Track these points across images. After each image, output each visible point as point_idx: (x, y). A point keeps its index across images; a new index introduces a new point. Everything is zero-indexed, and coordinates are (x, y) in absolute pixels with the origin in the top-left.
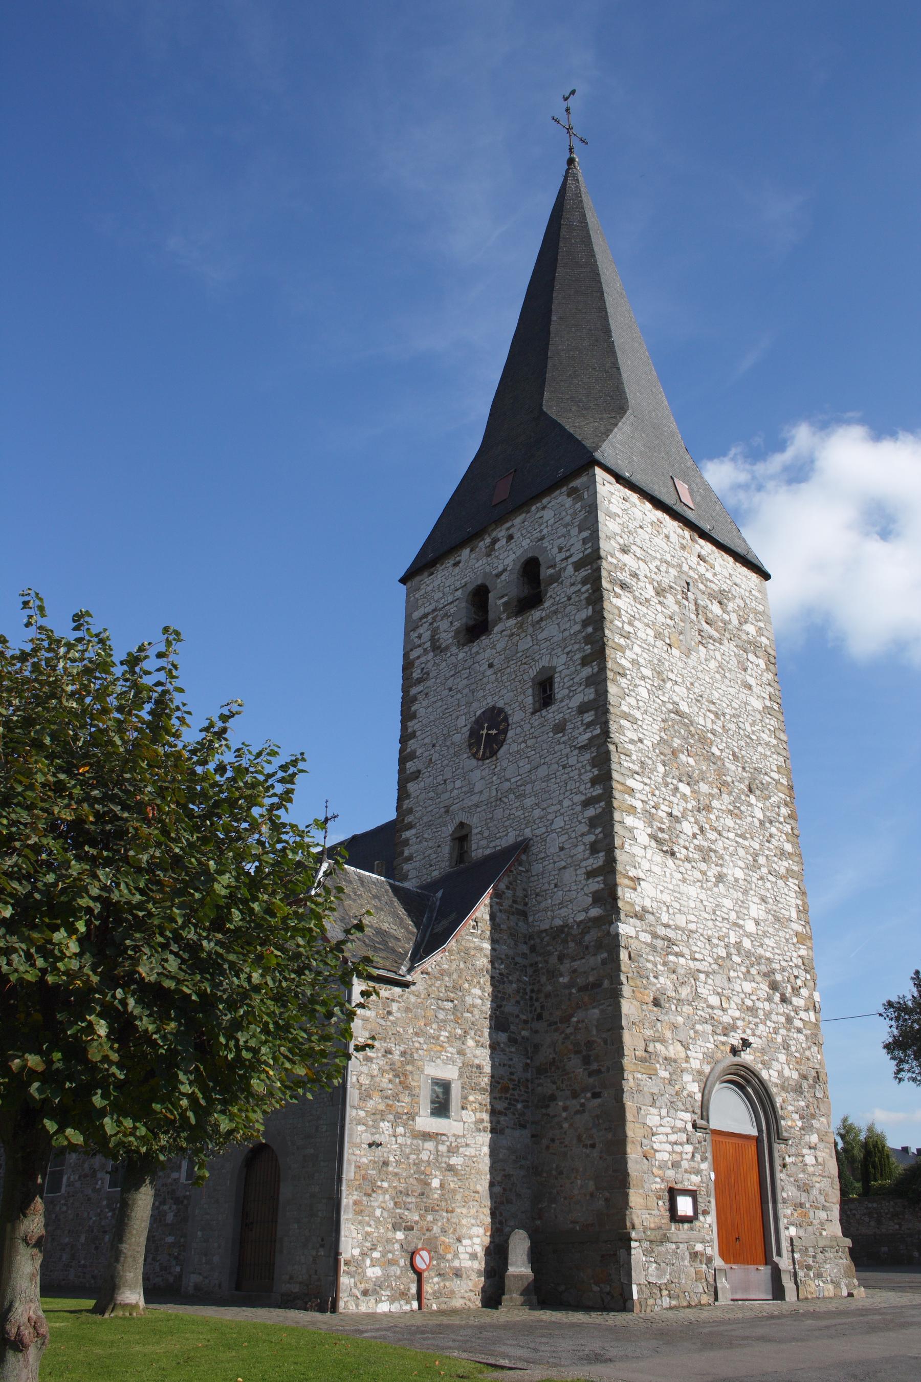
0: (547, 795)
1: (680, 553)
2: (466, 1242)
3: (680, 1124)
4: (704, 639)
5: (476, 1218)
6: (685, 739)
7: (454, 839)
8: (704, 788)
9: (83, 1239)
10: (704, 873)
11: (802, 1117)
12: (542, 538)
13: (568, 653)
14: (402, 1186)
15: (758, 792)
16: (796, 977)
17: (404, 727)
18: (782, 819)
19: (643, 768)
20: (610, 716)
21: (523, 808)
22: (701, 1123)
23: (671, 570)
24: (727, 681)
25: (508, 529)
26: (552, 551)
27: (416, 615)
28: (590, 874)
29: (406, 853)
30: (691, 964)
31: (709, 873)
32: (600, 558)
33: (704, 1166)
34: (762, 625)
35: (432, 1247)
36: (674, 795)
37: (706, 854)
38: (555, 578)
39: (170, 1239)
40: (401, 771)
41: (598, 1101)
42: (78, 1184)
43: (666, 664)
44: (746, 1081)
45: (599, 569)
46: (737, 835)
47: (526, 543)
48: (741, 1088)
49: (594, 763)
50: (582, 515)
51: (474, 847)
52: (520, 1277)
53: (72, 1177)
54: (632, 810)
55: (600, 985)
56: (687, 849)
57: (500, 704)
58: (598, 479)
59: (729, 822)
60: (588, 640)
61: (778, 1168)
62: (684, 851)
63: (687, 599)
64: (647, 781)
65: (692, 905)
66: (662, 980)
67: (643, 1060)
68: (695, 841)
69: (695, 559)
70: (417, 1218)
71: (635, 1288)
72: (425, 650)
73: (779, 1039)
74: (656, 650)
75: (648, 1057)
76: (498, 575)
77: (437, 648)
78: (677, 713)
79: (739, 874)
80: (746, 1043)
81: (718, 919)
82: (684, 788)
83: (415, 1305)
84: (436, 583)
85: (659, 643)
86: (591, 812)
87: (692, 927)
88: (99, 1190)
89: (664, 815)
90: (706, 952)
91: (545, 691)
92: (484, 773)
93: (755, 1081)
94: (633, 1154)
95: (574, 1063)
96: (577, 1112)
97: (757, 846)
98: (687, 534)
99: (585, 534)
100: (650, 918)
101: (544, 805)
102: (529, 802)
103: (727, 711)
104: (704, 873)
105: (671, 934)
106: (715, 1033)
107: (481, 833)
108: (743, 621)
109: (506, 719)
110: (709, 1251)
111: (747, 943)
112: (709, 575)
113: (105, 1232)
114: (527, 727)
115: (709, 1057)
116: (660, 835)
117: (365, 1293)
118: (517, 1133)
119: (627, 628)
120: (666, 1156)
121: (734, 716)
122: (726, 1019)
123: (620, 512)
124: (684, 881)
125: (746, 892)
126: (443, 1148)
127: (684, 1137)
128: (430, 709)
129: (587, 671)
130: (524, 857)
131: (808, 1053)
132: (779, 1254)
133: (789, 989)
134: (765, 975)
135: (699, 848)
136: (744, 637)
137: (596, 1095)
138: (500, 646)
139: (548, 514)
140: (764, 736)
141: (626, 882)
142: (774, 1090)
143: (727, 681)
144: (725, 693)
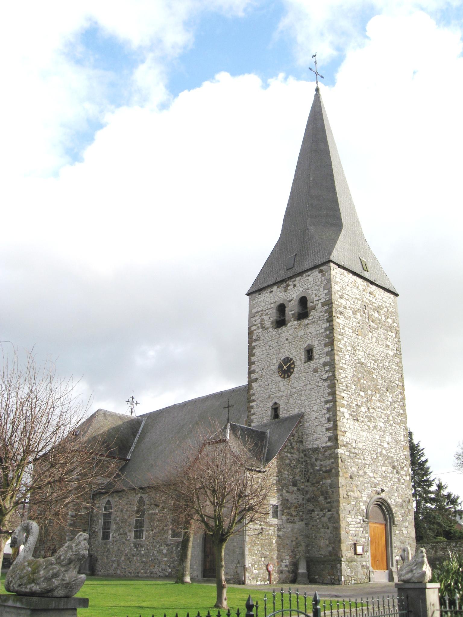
0: (310, 397)
2: (284, 561)
3: (358, 521)
6: (363, 373)
7: (272, 409)
8: (370, 392)
9: (123, 559)
11: (402, 517)
12: (308, 289)
15: (390, 391)
16: (402, 463)
17: (250, 359)
18: (399, 400)
19: (347, 388)
24: (379, 346)
25: (294, 281)
26: (312, 297)
27: (254, 311)
28: (328, 429)
29: (252, 412)
30: (363, 462)
31: (371, 426)
32: (332, 303)
34: (394, 318)
36: (358, 397)
38: (314, 308)
39: (166, 559)
40: (249, 377)
41: (330, 513)
42: (118, 537)
43: (356, 343)
45: (331, 308)
46: (381, 409)
50: (325, 283)
51: (281, 413)
53: (115, 535)
54: (343, 406)
57: (291, 357)
58: (332, 268)
59: (379, 405)
60: (327, 336)
61: (393, 535)
62: (362, 419)
63: (365, 313)
64: (349, 393)
65: (364, 439)
66: (353, 468)
68: (366, 414)
69: (368, 294)
71: (343, 577)
73: (395, 488)
74: (352, 338)
76: (290, 301)
77: (263, 327)
78: (360, 363)
79: (382, 425)
80: (383, 490)
82: (362, 394)
83: (268, 582)
84: (262, 299)
86: (328, 406)
87: (364, 447)
89: (354, 405)
90: (369, 457)
91: (309, 354)
92: (285, 384)
93: (386, 504)
94: (343, 532)
95: (321, 499)
96: (322, 516)
98: (365, 283)
99: (326, 291)
100: (349, 446)
101: (310, 400)
102: (303, 398)
103: (379, 358)
104: (369, 426)
105: (356, 451)
107: (283, 408)
110: (368, 564)
112: (374, 301)
113: (134, 556)
114: (302, 368)
115: (369, 496)
116: (353, 413)
117: (253, 578)
118: (300, 523)
119: (342, 331)
120: (353, 532)
122: (376, 481)
123: (339, 281)
124: (361, 430)
127: (360, 525)
128: (261, 353)
129: (327, 349)
130: (302, 420)
131: (406, 492)
132: (392, 566)
133: (400, 468)
135: (367, 417)
137: (329, 511)
138: (291, 332)
139: (310, 279)
140: (393, 366)
141: (341, 433)
142: (392, 507)
143: (379, 346)
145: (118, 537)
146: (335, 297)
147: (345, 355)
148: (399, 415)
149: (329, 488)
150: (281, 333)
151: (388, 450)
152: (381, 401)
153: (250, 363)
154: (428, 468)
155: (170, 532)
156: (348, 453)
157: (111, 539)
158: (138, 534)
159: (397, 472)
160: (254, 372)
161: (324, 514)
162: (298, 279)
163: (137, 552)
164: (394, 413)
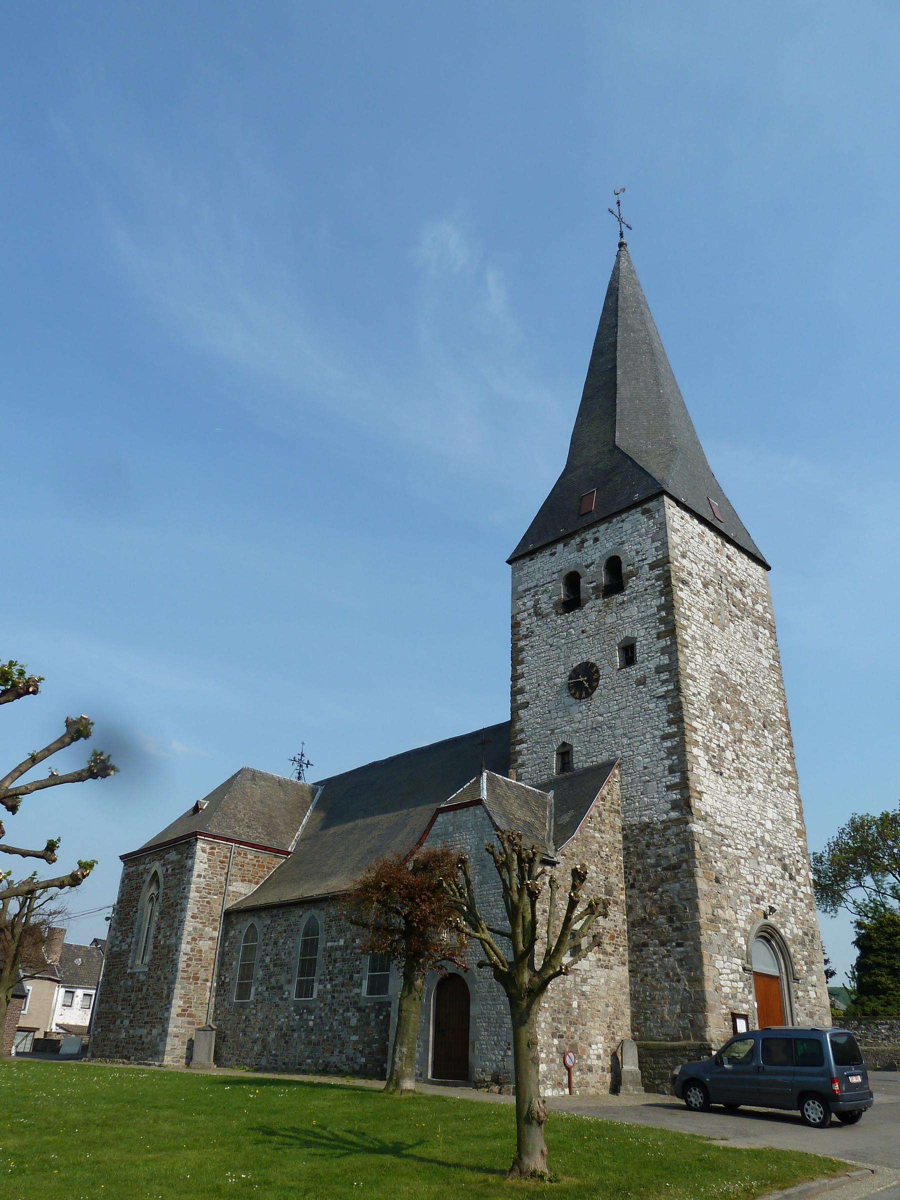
1: (716, 555)
2: (594, 1047)
3: (734, 967)
4: (733, 618)
5: (599, 1030)
9: (273, 1035)
10: (740, 787)
11: (806, 964)
13: (646, 629)
14: (556, 1007)
15: (769, 728)
16: (798, 861)
17: (514, 669)
20: (680, 677)
21: (614, 736)
22: (748, 966)
23: (711, 568)
25: (594, 533)
26: (628, 553)
27: (521, 588)
28: (669, 788)
29: (520, 761)
33: (751, 997)
35: (574, 1048)
37: (740, 773)
39: (355, 1038)
40: (513, 700)
44: (769, 935)
47: (609, 545)
48: (768, 941)
49: (670, 709)
52: (631, 1073)
53: (260, 989)
54: (696, 743)
55: (680, 867)
56: (729, 769)
57: (592, 660)
58: (666, 505)
59: (753, 750)
60: (662, 620)
62: (727, 771)
64: (704, 722)
67: (712, 921)
70: (565, 1029)
72: (529, 614)
75: (714, 920)
76: (587, 567)
77: (538, 613)
78: (720, 672)
79: (761, 787)
80: (772, 910)
81: (758, 824)
82: (726, 727)
83: (567, 1091)
84: (537, 566)
85: (707, 623)
86: (668, 744)
87: (735, 826)
88: (286, 999)
97: (770, 767)
99: (658, 544)
104: (740, 787)
106: (752, 901)
108: (755, 602)
109: (597, 671)
111: (767, 837)
112: (733, 570)
115: (751, 920)
119: (688, 613)
121: (753, 673)
122: (758, 892)
123: (679, 527)
124: (728, 793)
125: (765, 801)
126: (578, 979)
129: (662, 643)
134: (780, 860)
135: (736, 770)
136: (756, 614)
137: (678, 945)
139: (627, 526)
141: (696, 794)
144: (746, 656)
145: (266, 994)
146: (674, 553)
147: (695, 654)
148: (785, 772)
149: (676, 900)
150: (573, 621)
151: (774, 833)
152: (757, 744)
153: (515, 678)
155: (365, 983)
156: (708, 834)
157: (252, 997)
158: (305, 990)
159: (791, 878)
160: (521, 691)
161: (668, 951)
162: (602, 528)
163: (301, 1023)
164: (778, 769)
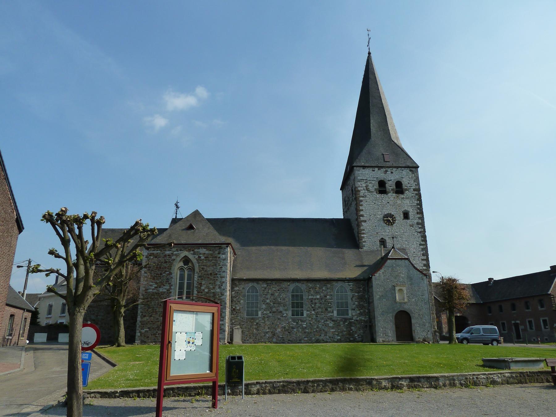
57: (392, 213)
129: (419, 216)
154: (47, 222)
